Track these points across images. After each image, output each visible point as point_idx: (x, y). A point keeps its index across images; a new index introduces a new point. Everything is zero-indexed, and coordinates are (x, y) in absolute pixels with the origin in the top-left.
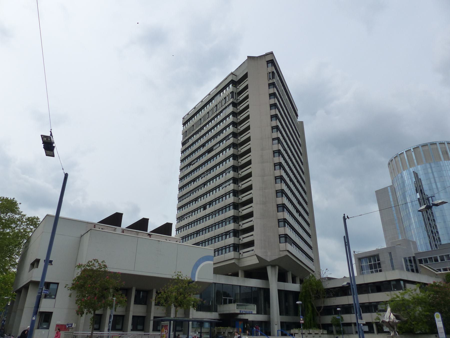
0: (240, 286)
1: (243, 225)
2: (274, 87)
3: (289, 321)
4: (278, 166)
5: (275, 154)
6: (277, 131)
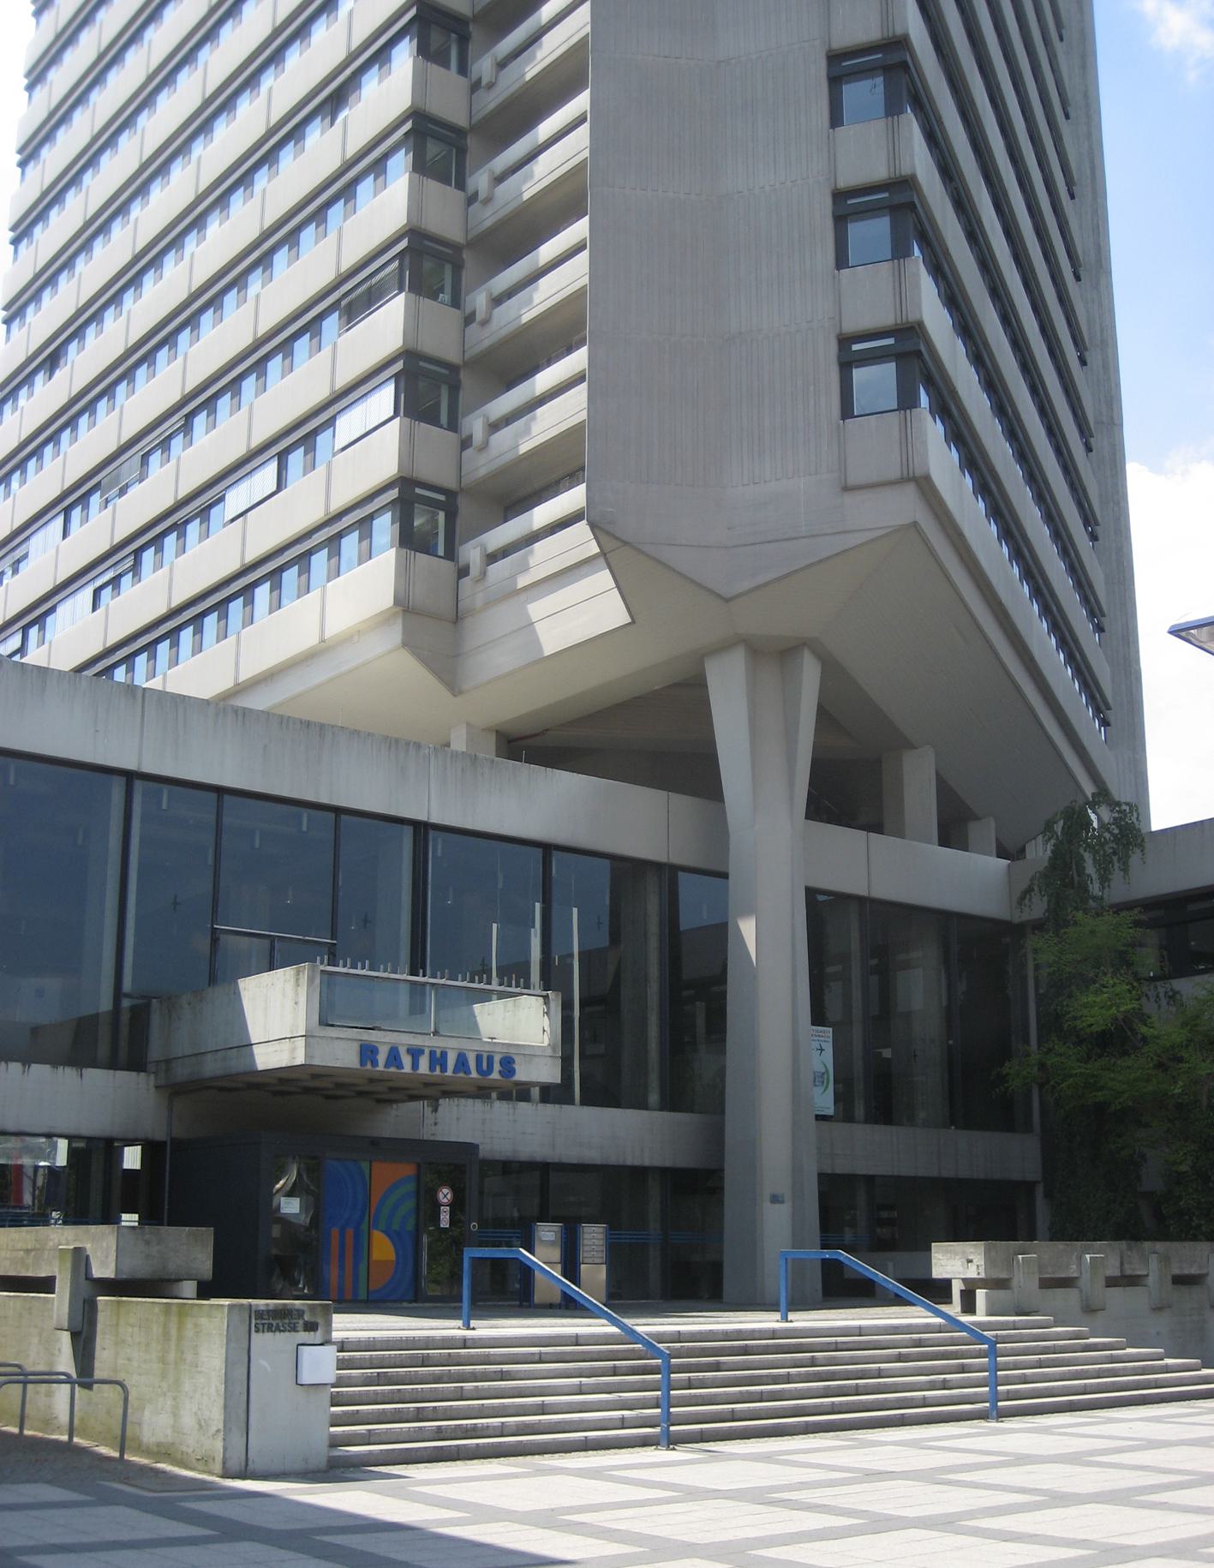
0: (422, 830)
1: (496, 311)
2: (892, 109)
3: (905, 1169)
4: (889, 370)
5: (857, 231)
6: (892, 109)
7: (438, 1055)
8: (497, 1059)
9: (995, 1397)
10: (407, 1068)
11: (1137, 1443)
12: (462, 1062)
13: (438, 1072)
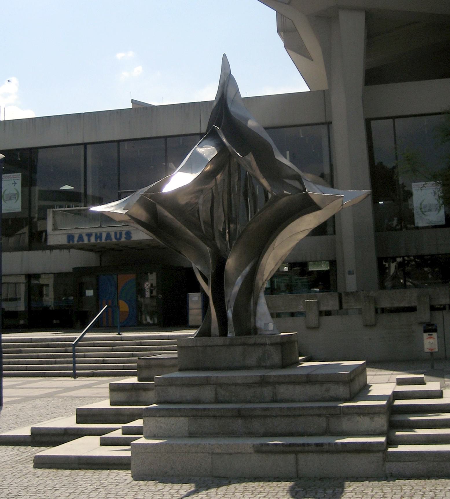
7: (98, 234)
9: (74, 369)
10: (86, 241)
11: (61, 389)
12: (108, 236)
13: (99, 241)
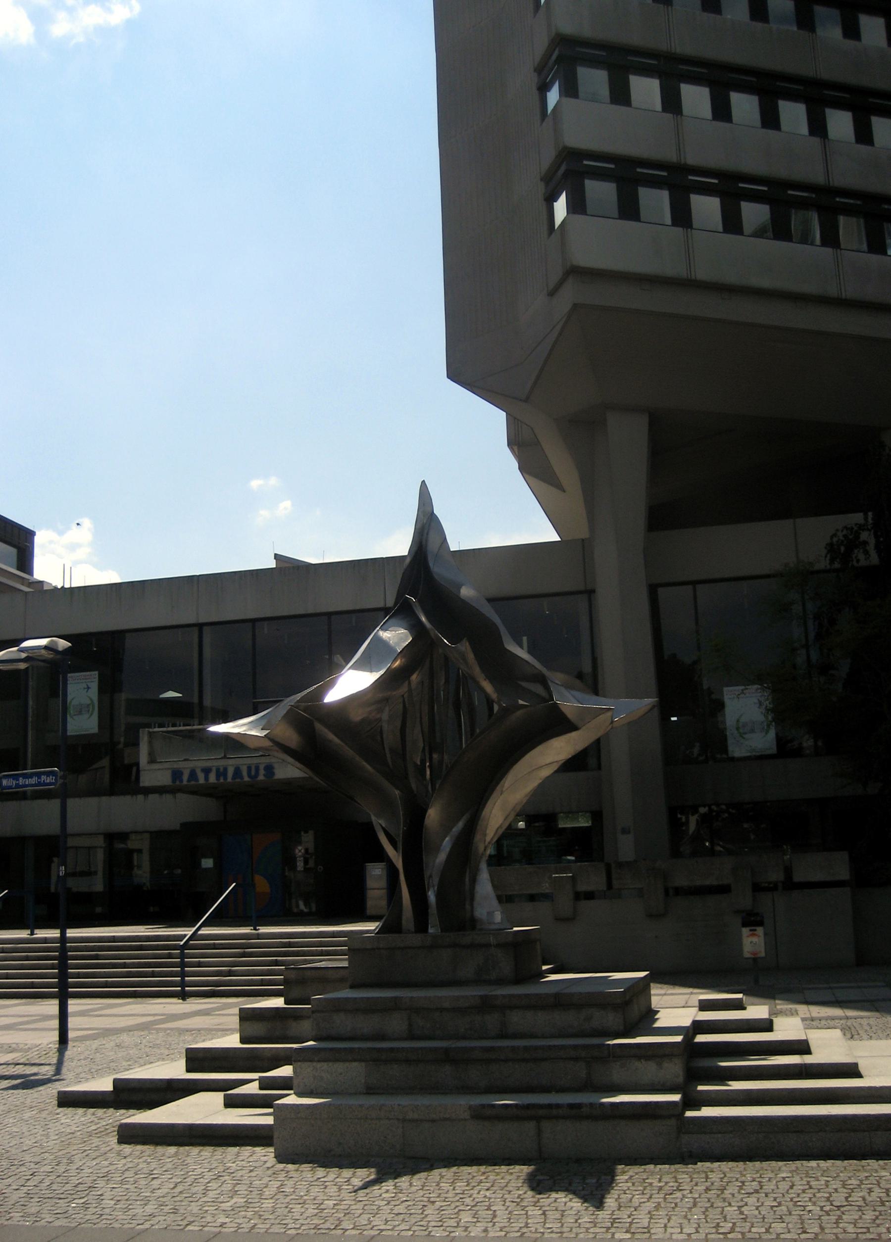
7: (222, 769)
8: (262, 767)
11: (94, 1032)
13: (222, 780)
